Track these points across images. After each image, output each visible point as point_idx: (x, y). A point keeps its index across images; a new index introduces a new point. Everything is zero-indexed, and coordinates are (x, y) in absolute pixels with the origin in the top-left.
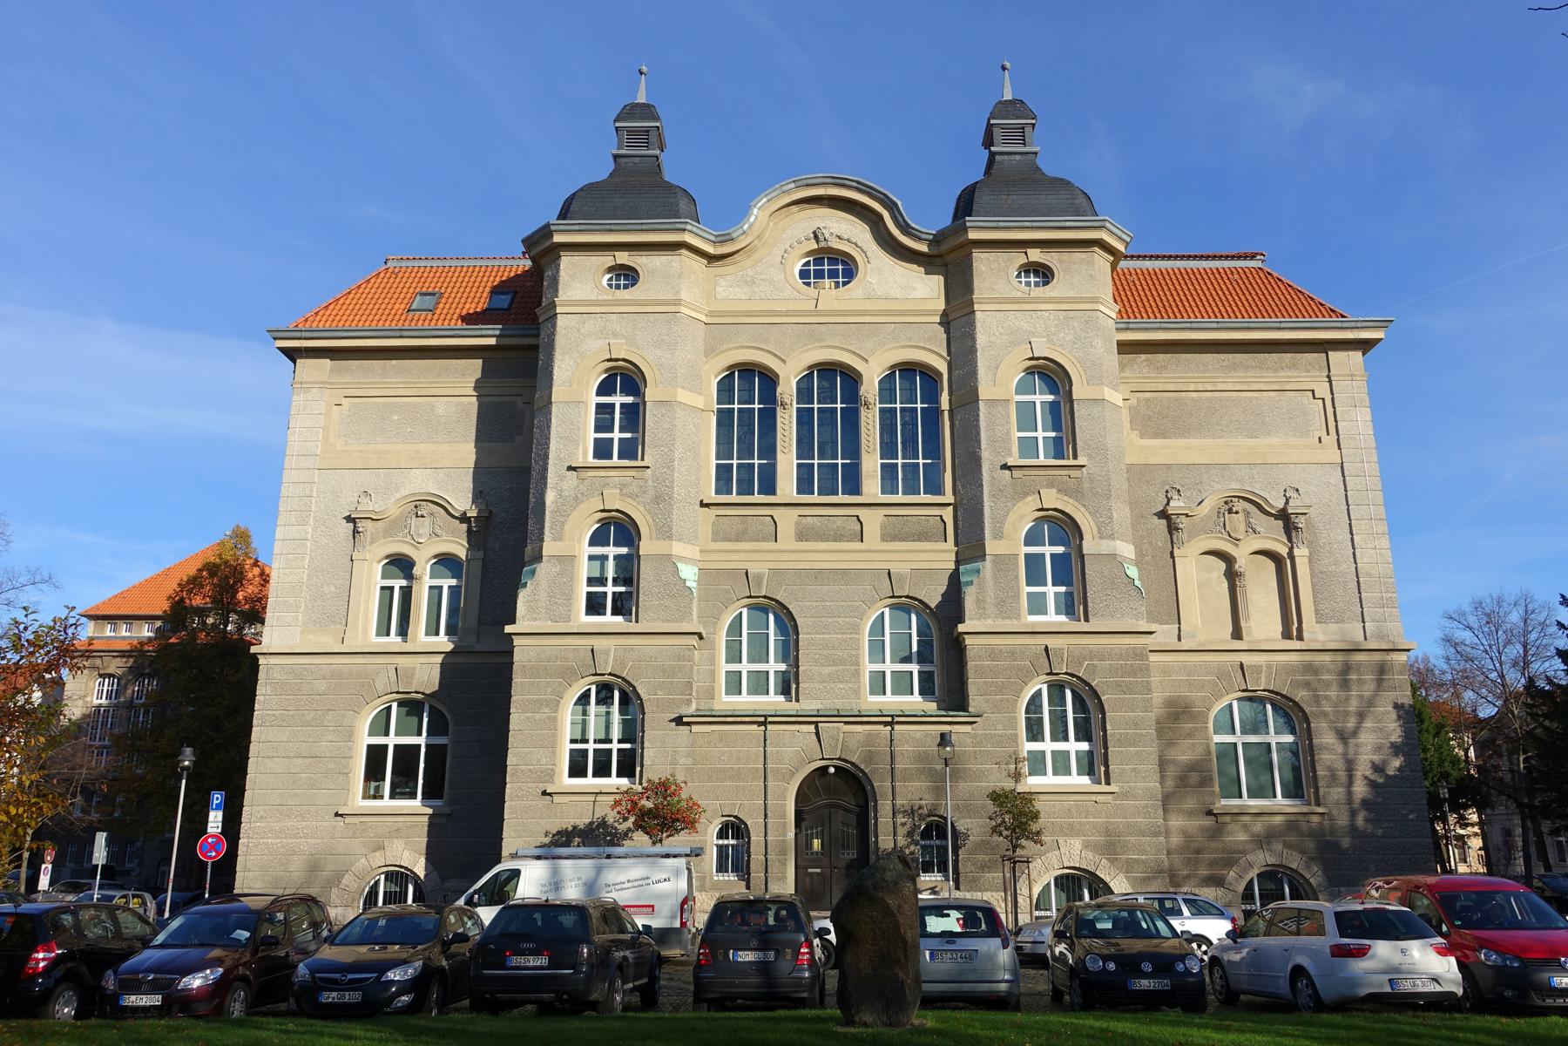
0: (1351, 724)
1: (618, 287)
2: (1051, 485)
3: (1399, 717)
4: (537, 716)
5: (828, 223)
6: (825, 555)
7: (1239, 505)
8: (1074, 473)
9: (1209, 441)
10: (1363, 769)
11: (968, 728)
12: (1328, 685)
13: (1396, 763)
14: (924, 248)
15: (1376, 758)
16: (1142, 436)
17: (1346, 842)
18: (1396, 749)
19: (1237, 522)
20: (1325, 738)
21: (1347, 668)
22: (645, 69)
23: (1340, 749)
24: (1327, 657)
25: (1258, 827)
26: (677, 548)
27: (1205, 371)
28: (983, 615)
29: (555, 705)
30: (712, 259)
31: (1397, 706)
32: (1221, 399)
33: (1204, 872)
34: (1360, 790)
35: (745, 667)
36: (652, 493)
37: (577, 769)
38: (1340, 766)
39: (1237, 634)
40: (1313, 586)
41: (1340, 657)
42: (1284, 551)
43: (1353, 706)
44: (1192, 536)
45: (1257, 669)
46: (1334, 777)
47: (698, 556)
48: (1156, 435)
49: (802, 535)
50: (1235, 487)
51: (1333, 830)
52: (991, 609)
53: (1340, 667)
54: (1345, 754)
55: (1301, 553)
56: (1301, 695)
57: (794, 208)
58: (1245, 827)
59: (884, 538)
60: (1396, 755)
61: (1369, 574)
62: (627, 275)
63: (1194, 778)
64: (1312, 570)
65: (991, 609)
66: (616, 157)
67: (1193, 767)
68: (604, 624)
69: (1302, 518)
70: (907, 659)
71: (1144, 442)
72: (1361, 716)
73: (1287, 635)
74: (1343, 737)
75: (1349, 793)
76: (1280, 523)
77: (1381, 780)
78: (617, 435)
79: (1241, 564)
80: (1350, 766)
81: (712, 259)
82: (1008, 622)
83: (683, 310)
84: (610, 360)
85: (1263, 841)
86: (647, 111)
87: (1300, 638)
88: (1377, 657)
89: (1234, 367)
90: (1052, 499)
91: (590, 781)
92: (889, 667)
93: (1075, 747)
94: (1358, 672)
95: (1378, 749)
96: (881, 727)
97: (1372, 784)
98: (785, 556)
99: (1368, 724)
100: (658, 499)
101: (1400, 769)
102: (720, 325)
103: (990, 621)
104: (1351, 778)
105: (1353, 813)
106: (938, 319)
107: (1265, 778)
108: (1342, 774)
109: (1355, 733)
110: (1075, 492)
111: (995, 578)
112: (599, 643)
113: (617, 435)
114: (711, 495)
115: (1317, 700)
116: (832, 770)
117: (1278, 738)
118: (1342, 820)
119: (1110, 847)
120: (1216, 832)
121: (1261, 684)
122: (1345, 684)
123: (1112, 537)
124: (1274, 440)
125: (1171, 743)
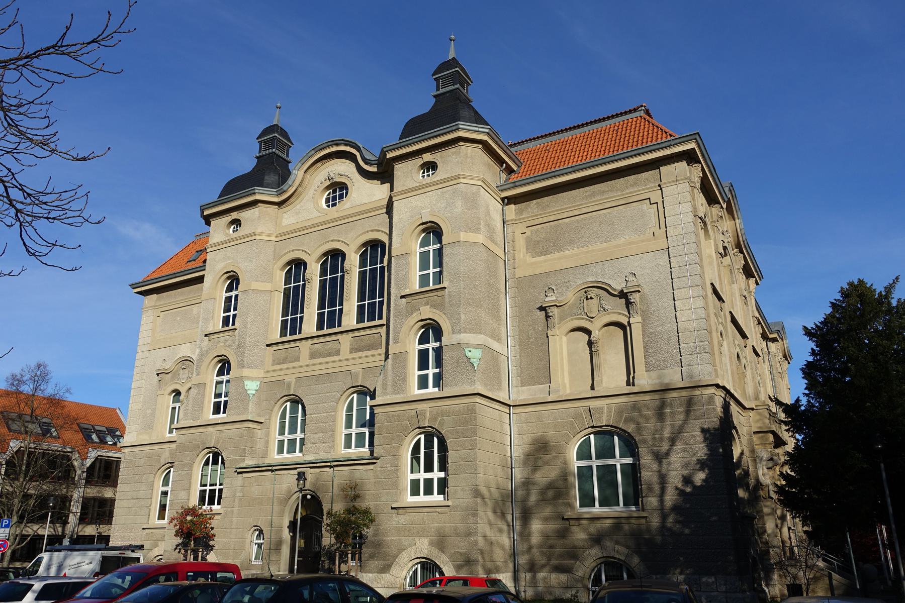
0: (664, 448)
1: (428, 175)
2: (427, 304)
3: (705, 439)
4: (183, 473)
5: (329, 169)
6: (322, 365)
7: (593, 293)
8: (439, 293)
9: (576, 251)
10: (675, 479)
11: (371, 467)
12: (647, 419)
13: (700, 477)
14: (374, 169)
15: (685, 472)
16: (533, 256)
17: (659, 539)
18: (702, 465)
19: (593, 305)
20: (646, 459)
21: (663, 405)
22: (453, 37)
23: (655, 466)
24: (647, 397)
25: (593, 529)
26: (246, 372)
27: (574, 202)
28: (385, 394)
29: (191, 466)
30: (280, 204)
31: (703, 431)
32: (578, 221)
33: (554, 562)
34: (670, 498)
35: (287, 437)
36: (237, 343)
37: (415, 492)
38: (655, 479)
39: (593, 388)
40: (645, 343)
41: (657, 396)
42: (624, 321)
43: (667, 432)
44: (562, 319)
45: (600, 410)
46: (650, 489)
47: (262, 375)
48: (542, 254)
49: (313, 356)
50: (580, 281)
51: (648, 530)
52: (390, 389)
53: (657, 403)
54: (659, 471)
55: (636, 320)
56: (630, 428)
57: (319, 164)
58: (585, 530)
59: (351, 352)
60: (702, 469)
61: (687, 330)
62: (431, 166)
63: (550, 493)
64: (644, 331)
65: (390, 389)
66: (435, 96)
67: (550, 486)
68: (431, 393)
69: (637, 295)
70: (363, 426)
71: (534, 260)
72: (673, 441)
73: (628, 384)
74: (659, 458)
75: (662, 501)
76: (623, 300)
77: (688, 490)
78: (431, 271)
79: (595, 335)
80: (663, 479)
81: (280, 204)
82: (398, 396)
83: (257, 237)
84: (422, 224)
85: (597, 540)
86: (454, 63)
87: (634, 385)
88: (684, 393)
89: (594, 194)
90: (427, 312)
91: (422, 498)
92: (354, 430)
93: (436, 475)
94: (671, 406)
95: (686, 465)
96: (328, 469)
97: (681, 493)
98: (345, 363)
99: (678, 447)
100: (239, 346)
101: (704, 481)
102: (285, 236)
103: (388, 397)
104: (663, 490)
105: (664, 517)
106: (384, 210)
107: (609, 492)
108: (657, 488)
109: (667, 454)
110: (439, 306)
111: (393, 368)
112: (420, 406)
113: (431, 271)
114: (276, 336)
115: (639, 429)
116: (309, 497)
117: (619, 461)
118: (655, 522)
119: (440, 544)
120: (563, 533)
121: (604, 421)
122: (660, 415)
123: (459, 332)
124: (620, 241)
125: (535, 469)
